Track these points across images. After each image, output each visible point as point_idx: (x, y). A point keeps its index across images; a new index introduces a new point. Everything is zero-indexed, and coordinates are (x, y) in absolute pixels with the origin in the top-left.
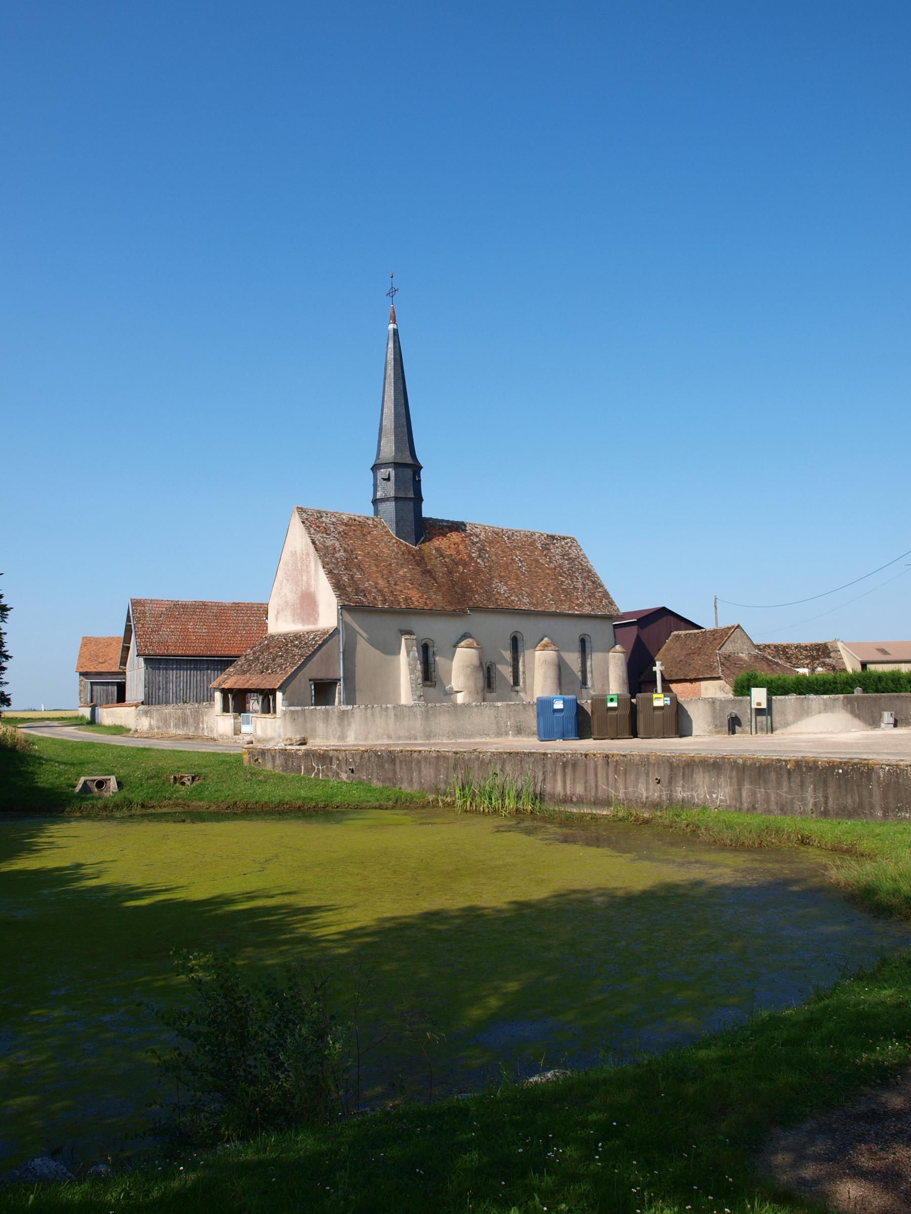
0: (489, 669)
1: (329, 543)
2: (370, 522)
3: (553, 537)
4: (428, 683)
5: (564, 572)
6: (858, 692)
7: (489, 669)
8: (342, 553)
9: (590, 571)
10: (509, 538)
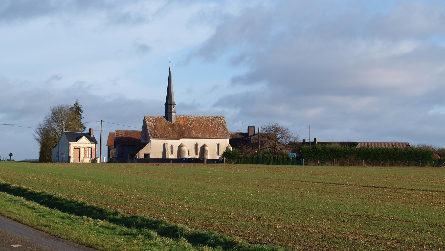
0: (189, 151)
3: (216, 117)
7: (189, 151)
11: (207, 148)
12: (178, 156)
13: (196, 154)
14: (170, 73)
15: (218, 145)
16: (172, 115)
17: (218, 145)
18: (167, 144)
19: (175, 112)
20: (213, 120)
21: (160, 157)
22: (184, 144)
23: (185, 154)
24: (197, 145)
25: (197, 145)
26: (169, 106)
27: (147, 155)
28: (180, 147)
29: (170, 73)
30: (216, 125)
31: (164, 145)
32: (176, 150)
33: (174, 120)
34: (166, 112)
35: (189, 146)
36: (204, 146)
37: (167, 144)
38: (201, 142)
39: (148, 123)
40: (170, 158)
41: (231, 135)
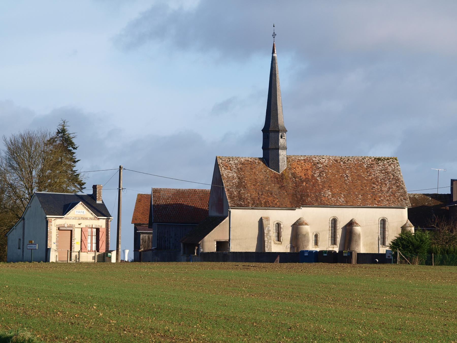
0: (316, 236)
1: (230, 175)
2: (257, 161)
3: (379, 159)
4: (278, 242)
5: (378, 182)
6: (274, 55)
8: (237, 180)
9: (398, 180)
10: (344, 163)
11: (358, 229)
12: (292, 247)
13: (334, 242)
14: (273, 59)
15: (383, 222)
16: (278, 155)
17: (383, 222)
18: (267, 219)
19: (285, 148)
20: (371, 166)
21: (253, 249)
22: (306, 219)
23: (308, 241)
24: (334, 222)
25: (334, 222)
26: (272, 135)
27: (222, 245)
28: (297, 226)
29: (273, 59)
30: (377, 178)
31: (261, 222)
32: (287, 234)
33: (283, 165)
34: (265, 147)
35: (317, 223)
36: (351, 224)
37: (267, 219)
38: (344, 215)
39: (224, 172)
40: (273, 251)
41: (413, 199)
